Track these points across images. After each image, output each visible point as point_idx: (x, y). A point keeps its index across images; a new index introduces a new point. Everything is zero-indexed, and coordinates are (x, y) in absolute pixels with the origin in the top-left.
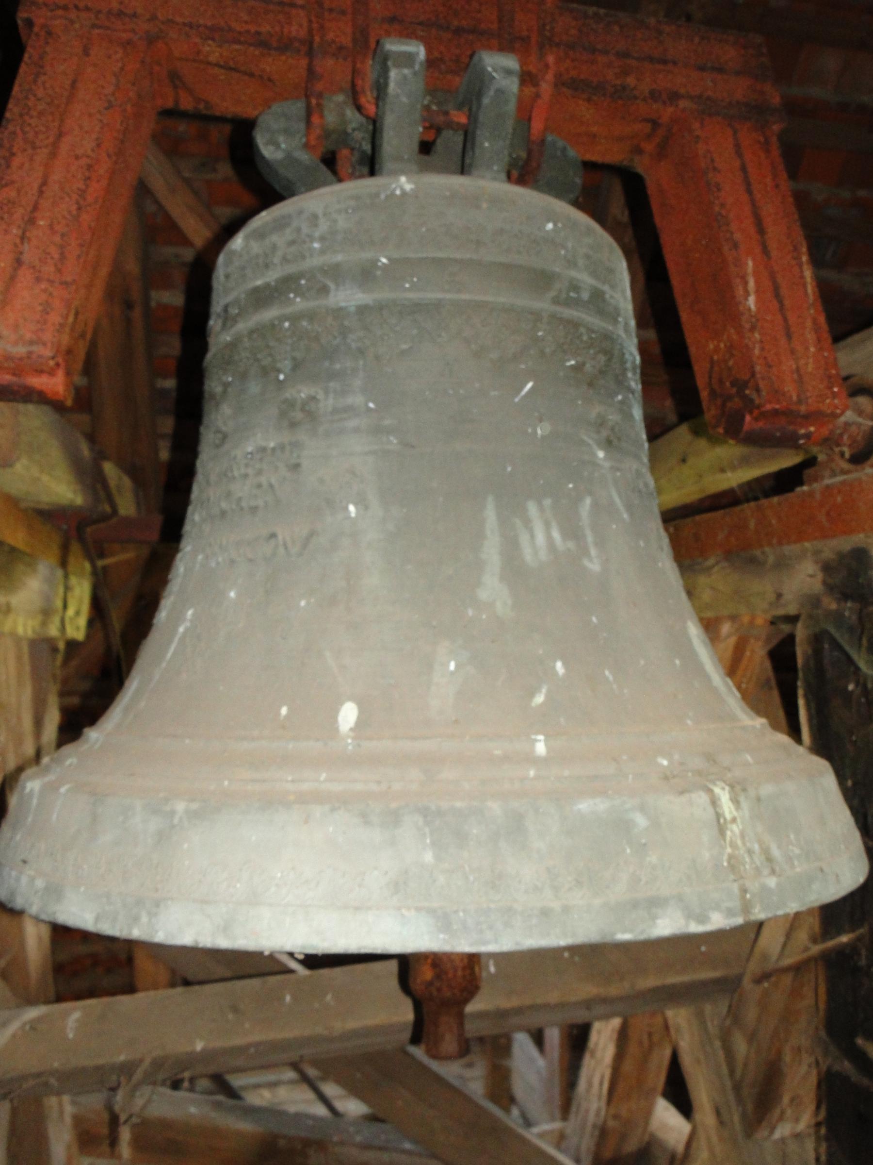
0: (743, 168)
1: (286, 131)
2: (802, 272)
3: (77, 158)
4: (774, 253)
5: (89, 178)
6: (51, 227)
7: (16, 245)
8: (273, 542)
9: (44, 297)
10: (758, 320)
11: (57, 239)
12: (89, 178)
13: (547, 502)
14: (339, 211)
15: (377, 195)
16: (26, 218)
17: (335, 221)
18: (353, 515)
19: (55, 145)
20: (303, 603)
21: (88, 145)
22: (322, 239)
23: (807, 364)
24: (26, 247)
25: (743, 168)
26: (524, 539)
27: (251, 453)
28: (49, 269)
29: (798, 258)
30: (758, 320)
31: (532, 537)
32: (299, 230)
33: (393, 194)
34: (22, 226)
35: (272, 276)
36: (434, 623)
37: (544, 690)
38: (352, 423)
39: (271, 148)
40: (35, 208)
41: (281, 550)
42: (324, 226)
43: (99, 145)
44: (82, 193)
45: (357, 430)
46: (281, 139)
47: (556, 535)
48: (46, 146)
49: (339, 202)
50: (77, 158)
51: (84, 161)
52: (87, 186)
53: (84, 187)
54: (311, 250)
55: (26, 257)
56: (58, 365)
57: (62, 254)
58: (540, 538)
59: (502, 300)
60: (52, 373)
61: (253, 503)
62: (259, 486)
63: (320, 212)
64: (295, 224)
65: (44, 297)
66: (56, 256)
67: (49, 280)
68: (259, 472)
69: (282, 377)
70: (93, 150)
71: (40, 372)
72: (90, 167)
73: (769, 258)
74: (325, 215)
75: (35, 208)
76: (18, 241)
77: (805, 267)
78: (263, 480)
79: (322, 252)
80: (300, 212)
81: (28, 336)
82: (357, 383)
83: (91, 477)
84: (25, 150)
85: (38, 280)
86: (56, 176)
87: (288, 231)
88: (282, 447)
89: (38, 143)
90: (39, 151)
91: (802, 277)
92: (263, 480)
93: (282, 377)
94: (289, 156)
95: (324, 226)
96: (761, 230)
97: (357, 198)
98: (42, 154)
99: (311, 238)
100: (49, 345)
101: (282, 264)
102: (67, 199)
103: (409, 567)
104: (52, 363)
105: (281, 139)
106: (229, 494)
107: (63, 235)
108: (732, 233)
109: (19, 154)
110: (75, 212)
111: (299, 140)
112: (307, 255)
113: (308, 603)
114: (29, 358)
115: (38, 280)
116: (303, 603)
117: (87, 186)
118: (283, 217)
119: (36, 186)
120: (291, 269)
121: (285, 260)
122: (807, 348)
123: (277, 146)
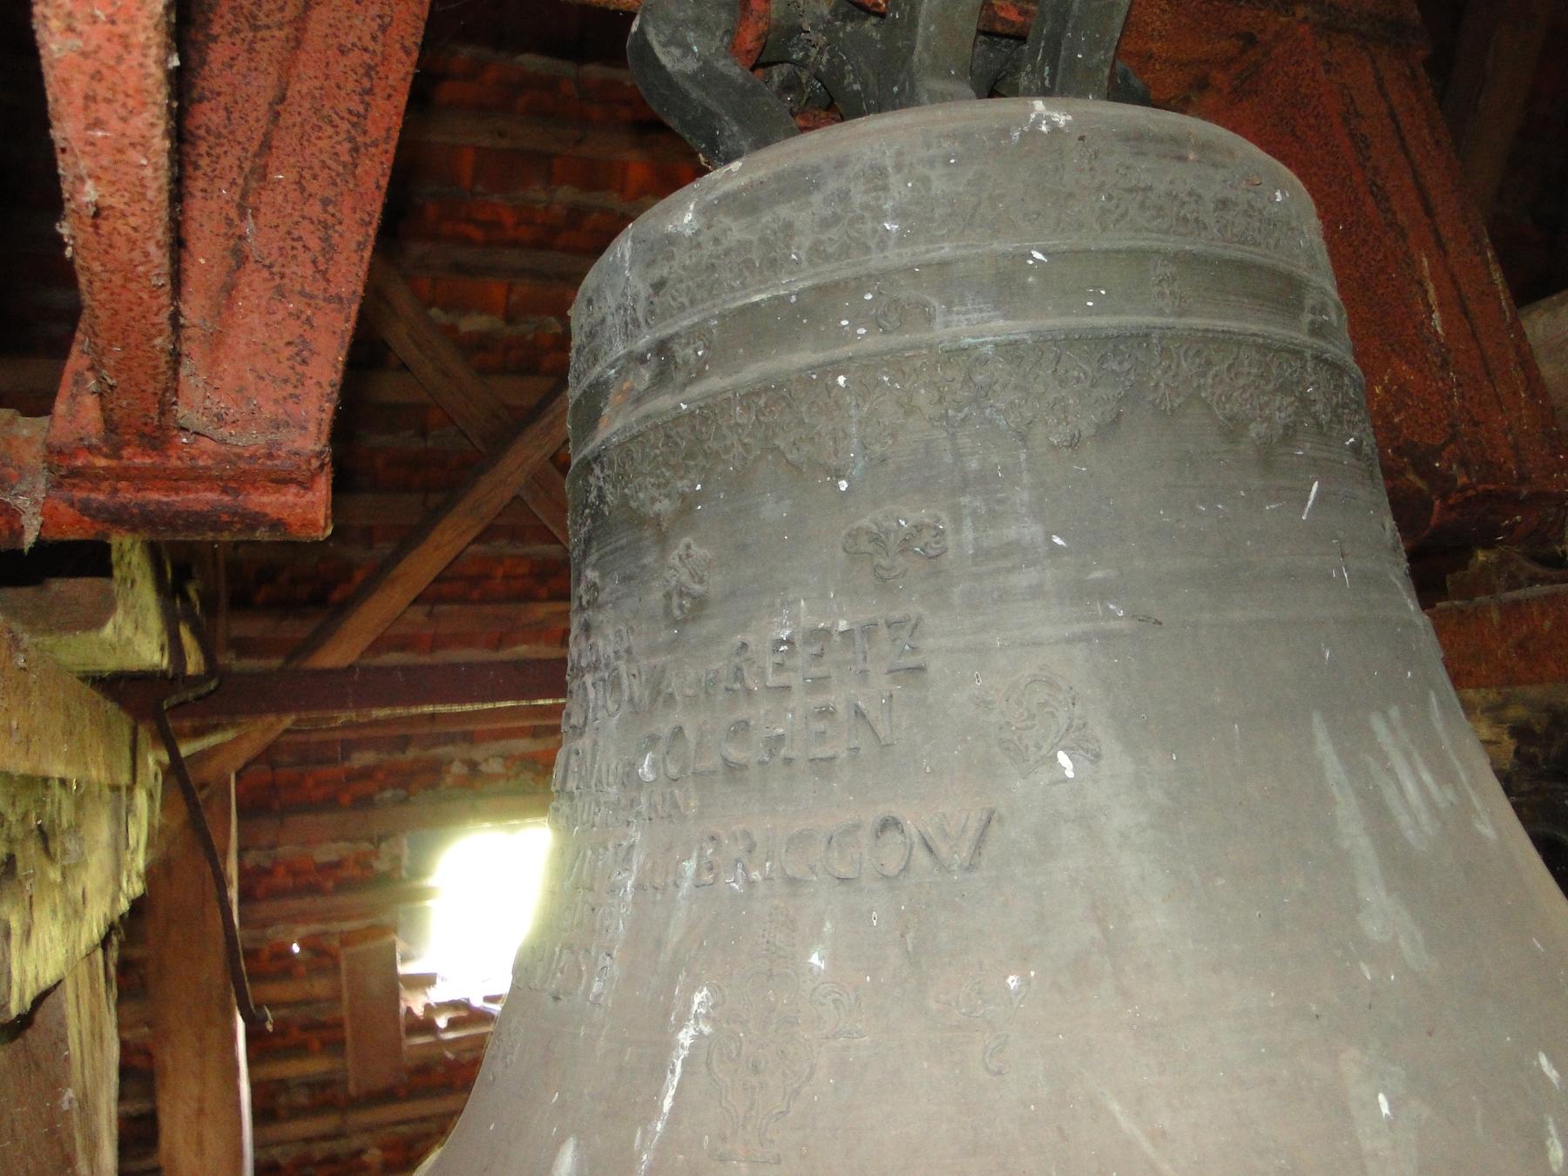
0: (1393, 116)
1: (698, 23)
2: (1490, 274)
3: (343, 51)
4: (1451, 247)
5: (370, 92)
6: (300, 184)
7: (229, 222)
8: (893, 837)
9: (295, 329)
10: (1449, 351)
11: (315, 210)
12: (370, 92)
13: (1394, 712)
14: (931, 163)
15: (1005, 133)
16: (247, 166)
17: (925, 180)
18: (1070, 774)
19: (300, 23)
20: (1013, 981)
21: (363, 26)
22: (900, 214)
23: (1519, 419)
24: (249, 227)
25: (1393, 116)
26: (1390, 793)
27: (789, 642)
28: (301, 269)
29: (1482, 253)
30: (1449, 351)
31: (1401, 790)
32: (844, 196)
33: (1035, 131)
34: (240, 181)
35: (790, 285)
36: (1314, 1008)
37: (1552, 1129)
38: (1023, 579)
39: (677, 52)
40: (266, 146)
41: (921, 857)
42: (900, 189)
43: (383, 28)
44: (358, 120)
45: (1036, 592)
46: (691, 36)
47: (1427, 777)
48: (280, 27)
49: (928, 146)
50: (343, 51)
51: (355, 57)
52: (367, 106)
53: (361, 109)
54: (883, 239)
55: (253, 245)
56: (322, 466)
57: (326, 240)
58: (1410, 787)
59: (1253, 328)
60: (306, 485)
61: (820, 752)
62: (826, 713)
63: (889, 163)
64: (832, 185)
65: (296, 328)
66: (314, 243)
67: (302, 293)
68: (819, 684)
69: (843, 485)
70: (374, 38)
71: (281, 481)
72: (369, 70)
73: (1446, 253)
74: (898, 168)
75: (266, 146)
76: (233, 214)
77: (1492, 267)
78: (836, 698)
79: (901, 240)
80: (841, 164)
81: (268, 410)
82: (1022, 496)
83: (175, 647)
84: (237, 31)
85: (281, 293)
86: (305, 83)
87: (817, 198)
88: (869, 630)
89: (263, 20)
90: (265, 33)
91: (1492, 283)
92: (836, 698)
93: (843, 485)
94: (706, 65)
95: (900, 189)
96: (1429, 211)
97: (966, 137)
98: (274, 40)
99: (880, 216)
100: (312, 428)
101: (810, 262)
102: (330, 131)
103: (1220, 882)
104: (315, 463)
105: (691, 36)
106: (741, 729)
107: (325, 202)
108: (1394, 214)
109: (225, 38)
110: (346, 158)
111: (716, 43)
112: (872, 244)
113: (1025, 981)
114: (270, 456)
115: (281, 293)
116: (1013, 981)
117: (367, 106)
118: (802, 172)
119: (262, 103)
120: (830, 272)
121: (816, 251)
122: (1515, 393)
123: (687, 49)
